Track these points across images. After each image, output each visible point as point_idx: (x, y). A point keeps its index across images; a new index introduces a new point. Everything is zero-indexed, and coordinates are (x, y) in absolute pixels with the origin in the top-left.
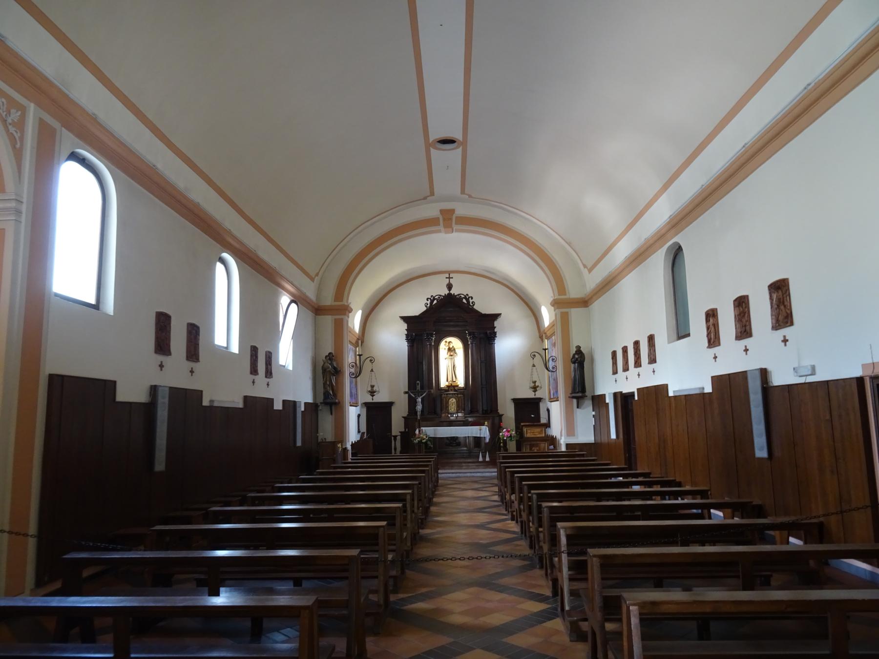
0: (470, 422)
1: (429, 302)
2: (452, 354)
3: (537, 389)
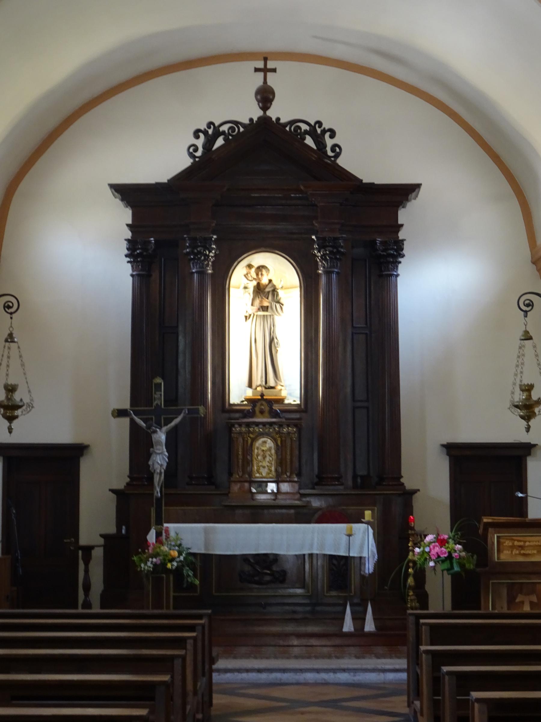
0: (318, 509)
1: (200, 142)
2: (266, 304)
3: (536, 410)
